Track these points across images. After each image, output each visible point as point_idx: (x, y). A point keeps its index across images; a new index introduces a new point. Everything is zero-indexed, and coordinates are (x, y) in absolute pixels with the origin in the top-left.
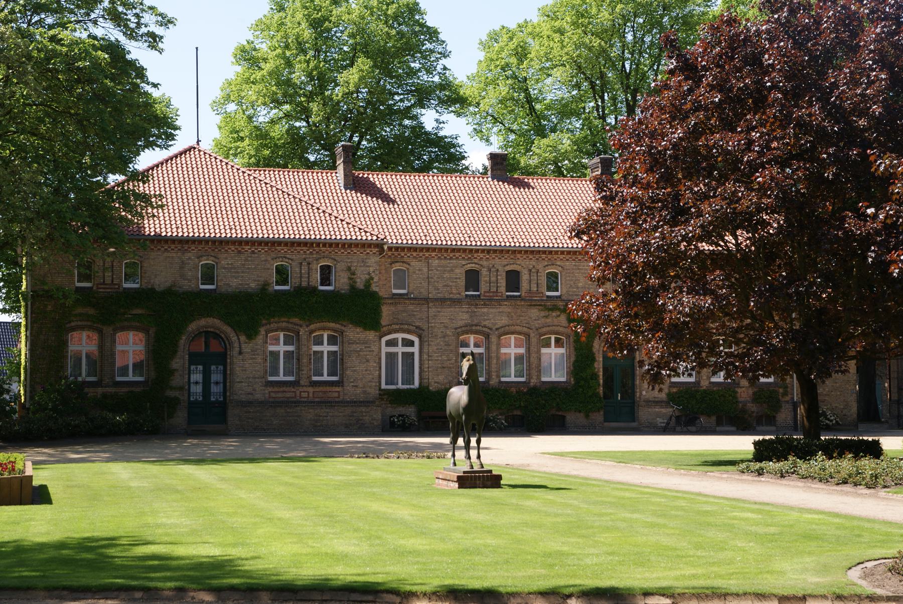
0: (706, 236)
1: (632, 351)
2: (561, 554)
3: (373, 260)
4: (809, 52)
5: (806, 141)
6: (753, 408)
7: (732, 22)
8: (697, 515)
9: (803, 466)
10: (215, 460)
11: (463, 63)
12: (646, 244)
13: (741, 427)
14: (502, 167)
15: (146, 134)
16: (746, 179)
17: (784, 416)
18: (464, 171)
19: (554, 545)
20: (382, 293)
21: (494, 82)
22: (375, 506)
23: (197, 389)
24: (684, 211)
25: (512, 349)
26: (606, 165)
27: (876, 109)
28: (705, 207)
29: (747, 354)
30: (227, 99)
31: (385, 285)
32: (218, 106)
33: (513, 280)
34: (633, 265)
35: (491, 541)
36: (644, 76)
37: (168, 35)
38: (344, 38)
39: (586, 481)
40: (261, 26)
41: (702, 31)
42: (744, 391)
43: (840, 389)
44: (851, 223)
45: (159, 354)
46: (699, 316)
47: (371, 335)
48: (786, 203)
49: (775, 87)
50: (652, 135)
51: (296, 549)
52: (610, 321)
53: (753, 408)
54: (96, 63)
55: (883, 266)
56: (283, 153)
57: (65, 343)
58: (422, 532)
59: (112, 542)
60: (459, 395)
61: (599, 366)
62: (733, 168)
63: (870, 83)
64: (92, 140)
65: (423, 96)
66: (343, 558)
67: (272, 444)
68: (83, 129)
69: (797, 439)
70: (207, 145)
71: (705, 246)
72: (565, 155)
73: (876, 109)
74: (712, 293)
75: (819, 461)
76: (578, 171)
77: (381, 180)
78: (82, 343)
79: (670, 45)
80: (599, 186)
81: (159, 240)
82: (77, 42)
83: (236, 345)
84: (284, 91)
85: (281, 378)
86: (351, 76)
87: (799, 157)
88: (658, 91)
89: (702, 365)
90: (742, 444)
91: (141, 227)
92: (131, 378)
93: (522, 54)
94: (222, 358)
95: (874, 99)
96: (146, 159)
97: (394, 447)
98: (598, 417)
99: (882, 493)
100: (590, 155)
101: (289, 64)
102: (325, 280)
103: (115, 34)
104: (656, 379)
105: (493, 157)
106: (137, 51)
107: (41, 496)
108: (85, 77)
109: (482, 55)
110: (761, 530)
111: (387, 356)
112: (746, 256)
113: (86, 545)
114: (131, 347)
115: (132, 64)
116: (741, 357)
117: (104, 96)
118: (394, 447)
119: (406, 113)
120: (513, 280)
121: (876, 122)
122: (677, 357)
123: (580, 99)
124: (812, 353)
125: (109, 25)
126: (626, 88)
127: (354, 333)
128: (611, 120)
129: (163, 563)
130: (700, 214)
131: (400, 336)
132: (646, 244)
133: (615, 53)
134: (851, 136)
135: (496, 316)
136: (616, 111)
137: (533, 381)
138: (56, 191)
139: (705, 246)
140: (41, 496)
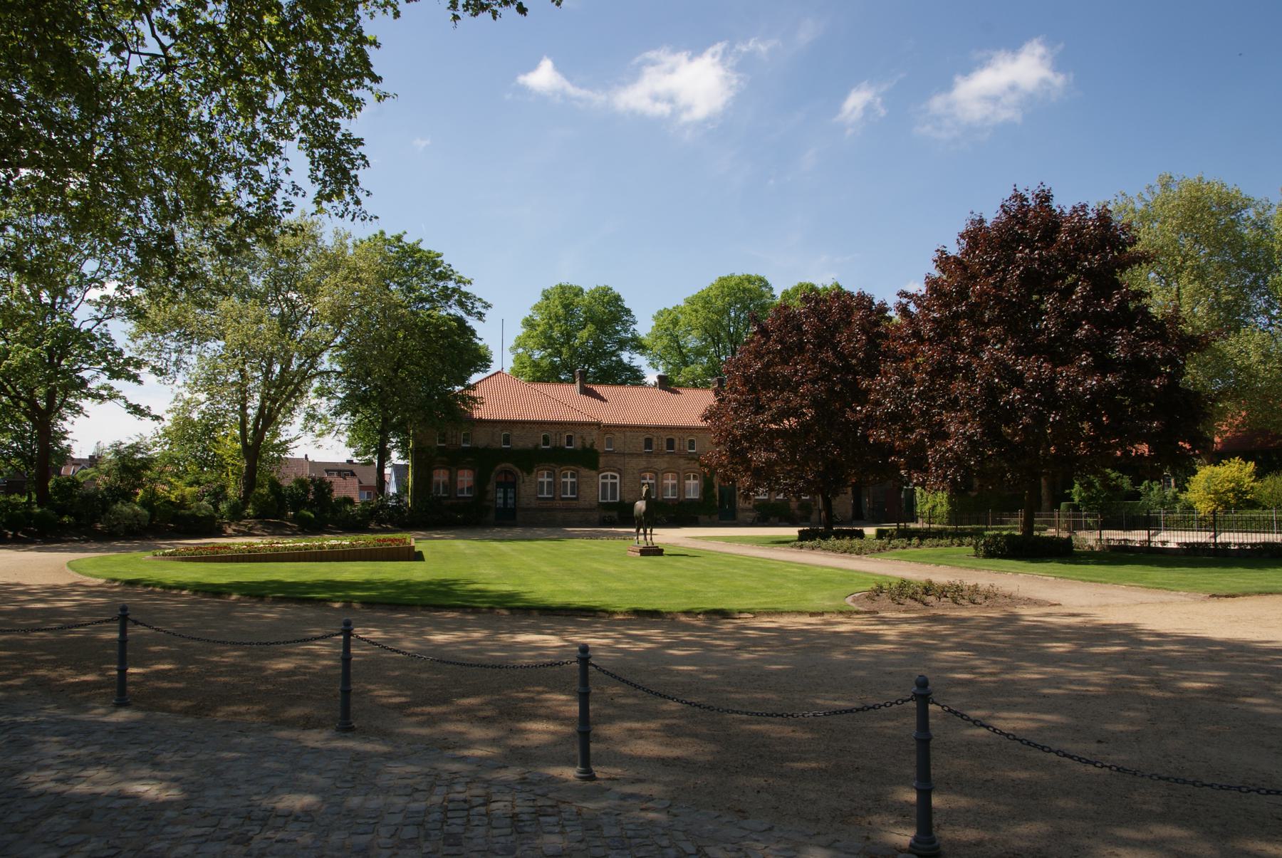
0: (773, 421)
1: (734, 482)
2: (695, 591)
3: (595, 432)
4: (825, 324)
5: (825, 371)
6: (798, 512)
7: (786, 307)
8: (768, 571)
9: (824, 543)
10: (510, 540)
11: (644, 327)
12: (742, 424)
13: (791, 523)
14: (664, 383)
15: (475, 365)
16: (794, 390)
17: (814, 517)
18: (644, 385)
19: (692, 586)
20: (600, 450)
21: (660, 337)
22: (595, 565)
23: (501, 501)
24: (762, 407)
25: (670, 481)
26: (721, 382)
27: (861, 355)
28: (773, 405)
29: (795, 484)
30: (518, 346)
31: (602, 447)
32: (513, 349)
33: (670, 443)
34: (735, 436)
35: (657, 584)
36: (740, 335)
37: (489, 314)
38: (581, 314)
39: (709, 552)
40: (537, 308)
41: (771, 312)
42: (794, 504)
43: (843, 503)
44: (848, 414)
45: (480, 482)
46: (770, 464)
47: (594, 473)
48: (815, 404)
49: (809, 342)
50: (745, 366)
51: (552, 587)
52: (721, 465)
53: (798, 512)
54: (450, 328)
55: (865, 437)
56: (546, 375)
57: (430, 477)
58: (620, 580)
59: (455, 582)
60: (641, 505)
61: (716, 490)
62: (788, 384)
63: (858, 341)
64: (448, 368)
65: (622, 344)
66: (578, 593)
67: (540, 531)
68: (443, 363)
69: (822, 528)
70: (507, 370)
71: (773, 426)
72: (698, 377)
73: (861, 355)
74: (777, 451)
75: (832, 541)
76: (705, 385)
77: (599, 389)
78: (440, 476)
79: (754, 319)
80: (717, 393)
81: (481, 421)
82: (441, 317)
84: (548, 342)
85: (545, 495)
86: (584, 334)
87: (822, 379)
88: (748, 343)
89: (771, 490)
90: (793, 532)
91: (472, 414)
92: (466, 495)
93: (675, 322)
94: (514, 485)
95: (859, 349)
96: (475, 378)
97: (605, 534)
98: (716, 518)
99: (864, 557)
100: (712, 377)
101: (551, 327)
102: (569, 443)
103: (460, 313)
104: (747, 497)
105: (659, 377)
106: (472, 322)
107: (419, 557)
108: (445, 335)
109: (654, 323)
110: (802, 578)
111: (603, 484)
112: (794, 431)
113: (442, 583)
114: (465, 478)
115: (469, 328)
116: (792, 485)
117: (453, 345)
118: (605, 534)
119: (613, 353)
120: (670, 443)
121: (861, 361)
122: (758, 485)
123: (706, 347)
124: (829, 484)
125: (458, 308)
126: (731, 341)
127: (585, 472)
128: (723, 358)
129: (482, 594)
130: (770, 409)
131: (609, 473)
132: (742, 424)
133: (725, 322)
134: (848, 369)
135: (661, 463)
136: (726, 354)
137: (915, 809)
138: (428, 395)
139: (773, 426)
140: (419, 557)
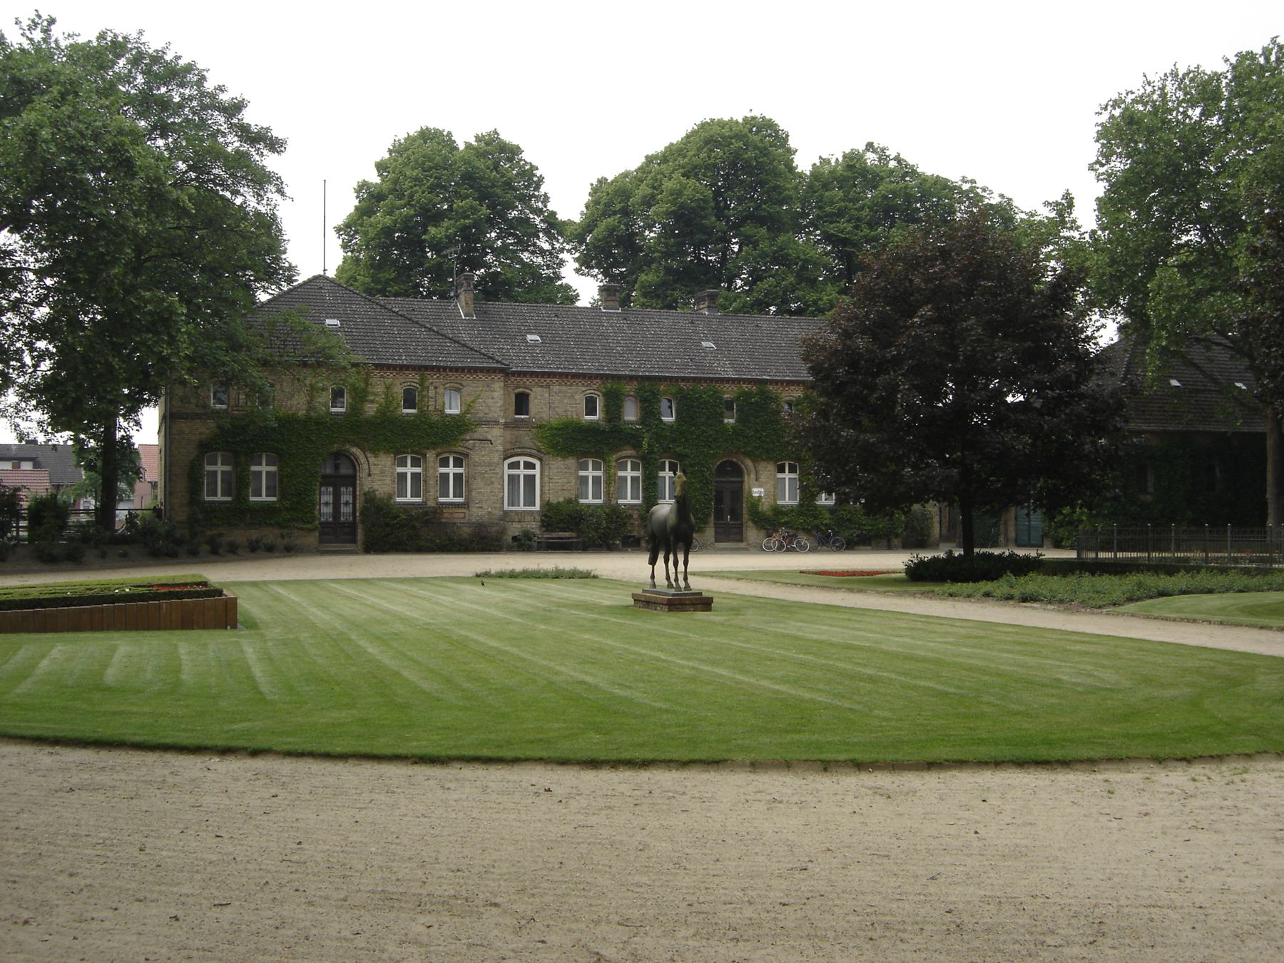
83: (365, 466)
90: (896, 561)
131: (522, 459)
